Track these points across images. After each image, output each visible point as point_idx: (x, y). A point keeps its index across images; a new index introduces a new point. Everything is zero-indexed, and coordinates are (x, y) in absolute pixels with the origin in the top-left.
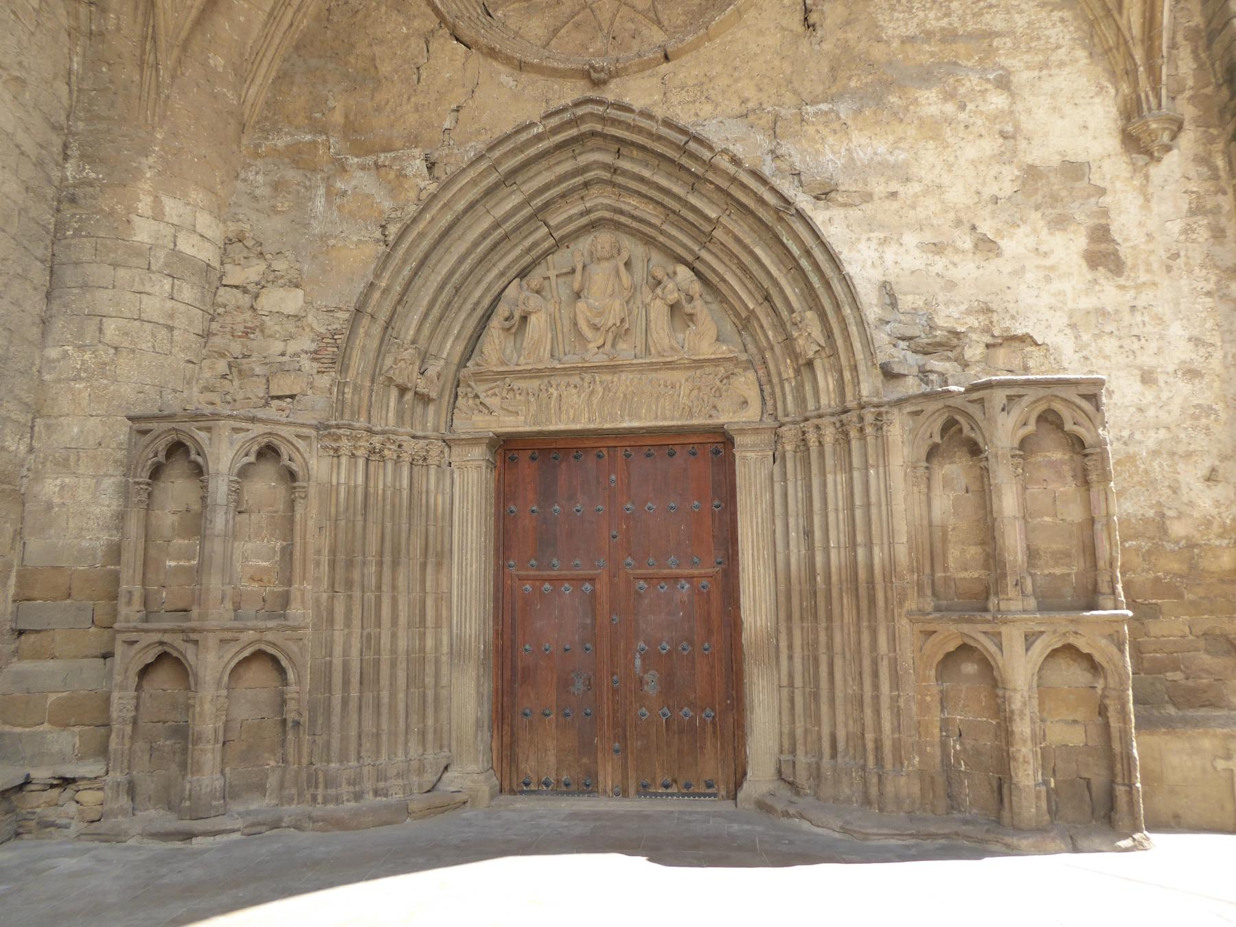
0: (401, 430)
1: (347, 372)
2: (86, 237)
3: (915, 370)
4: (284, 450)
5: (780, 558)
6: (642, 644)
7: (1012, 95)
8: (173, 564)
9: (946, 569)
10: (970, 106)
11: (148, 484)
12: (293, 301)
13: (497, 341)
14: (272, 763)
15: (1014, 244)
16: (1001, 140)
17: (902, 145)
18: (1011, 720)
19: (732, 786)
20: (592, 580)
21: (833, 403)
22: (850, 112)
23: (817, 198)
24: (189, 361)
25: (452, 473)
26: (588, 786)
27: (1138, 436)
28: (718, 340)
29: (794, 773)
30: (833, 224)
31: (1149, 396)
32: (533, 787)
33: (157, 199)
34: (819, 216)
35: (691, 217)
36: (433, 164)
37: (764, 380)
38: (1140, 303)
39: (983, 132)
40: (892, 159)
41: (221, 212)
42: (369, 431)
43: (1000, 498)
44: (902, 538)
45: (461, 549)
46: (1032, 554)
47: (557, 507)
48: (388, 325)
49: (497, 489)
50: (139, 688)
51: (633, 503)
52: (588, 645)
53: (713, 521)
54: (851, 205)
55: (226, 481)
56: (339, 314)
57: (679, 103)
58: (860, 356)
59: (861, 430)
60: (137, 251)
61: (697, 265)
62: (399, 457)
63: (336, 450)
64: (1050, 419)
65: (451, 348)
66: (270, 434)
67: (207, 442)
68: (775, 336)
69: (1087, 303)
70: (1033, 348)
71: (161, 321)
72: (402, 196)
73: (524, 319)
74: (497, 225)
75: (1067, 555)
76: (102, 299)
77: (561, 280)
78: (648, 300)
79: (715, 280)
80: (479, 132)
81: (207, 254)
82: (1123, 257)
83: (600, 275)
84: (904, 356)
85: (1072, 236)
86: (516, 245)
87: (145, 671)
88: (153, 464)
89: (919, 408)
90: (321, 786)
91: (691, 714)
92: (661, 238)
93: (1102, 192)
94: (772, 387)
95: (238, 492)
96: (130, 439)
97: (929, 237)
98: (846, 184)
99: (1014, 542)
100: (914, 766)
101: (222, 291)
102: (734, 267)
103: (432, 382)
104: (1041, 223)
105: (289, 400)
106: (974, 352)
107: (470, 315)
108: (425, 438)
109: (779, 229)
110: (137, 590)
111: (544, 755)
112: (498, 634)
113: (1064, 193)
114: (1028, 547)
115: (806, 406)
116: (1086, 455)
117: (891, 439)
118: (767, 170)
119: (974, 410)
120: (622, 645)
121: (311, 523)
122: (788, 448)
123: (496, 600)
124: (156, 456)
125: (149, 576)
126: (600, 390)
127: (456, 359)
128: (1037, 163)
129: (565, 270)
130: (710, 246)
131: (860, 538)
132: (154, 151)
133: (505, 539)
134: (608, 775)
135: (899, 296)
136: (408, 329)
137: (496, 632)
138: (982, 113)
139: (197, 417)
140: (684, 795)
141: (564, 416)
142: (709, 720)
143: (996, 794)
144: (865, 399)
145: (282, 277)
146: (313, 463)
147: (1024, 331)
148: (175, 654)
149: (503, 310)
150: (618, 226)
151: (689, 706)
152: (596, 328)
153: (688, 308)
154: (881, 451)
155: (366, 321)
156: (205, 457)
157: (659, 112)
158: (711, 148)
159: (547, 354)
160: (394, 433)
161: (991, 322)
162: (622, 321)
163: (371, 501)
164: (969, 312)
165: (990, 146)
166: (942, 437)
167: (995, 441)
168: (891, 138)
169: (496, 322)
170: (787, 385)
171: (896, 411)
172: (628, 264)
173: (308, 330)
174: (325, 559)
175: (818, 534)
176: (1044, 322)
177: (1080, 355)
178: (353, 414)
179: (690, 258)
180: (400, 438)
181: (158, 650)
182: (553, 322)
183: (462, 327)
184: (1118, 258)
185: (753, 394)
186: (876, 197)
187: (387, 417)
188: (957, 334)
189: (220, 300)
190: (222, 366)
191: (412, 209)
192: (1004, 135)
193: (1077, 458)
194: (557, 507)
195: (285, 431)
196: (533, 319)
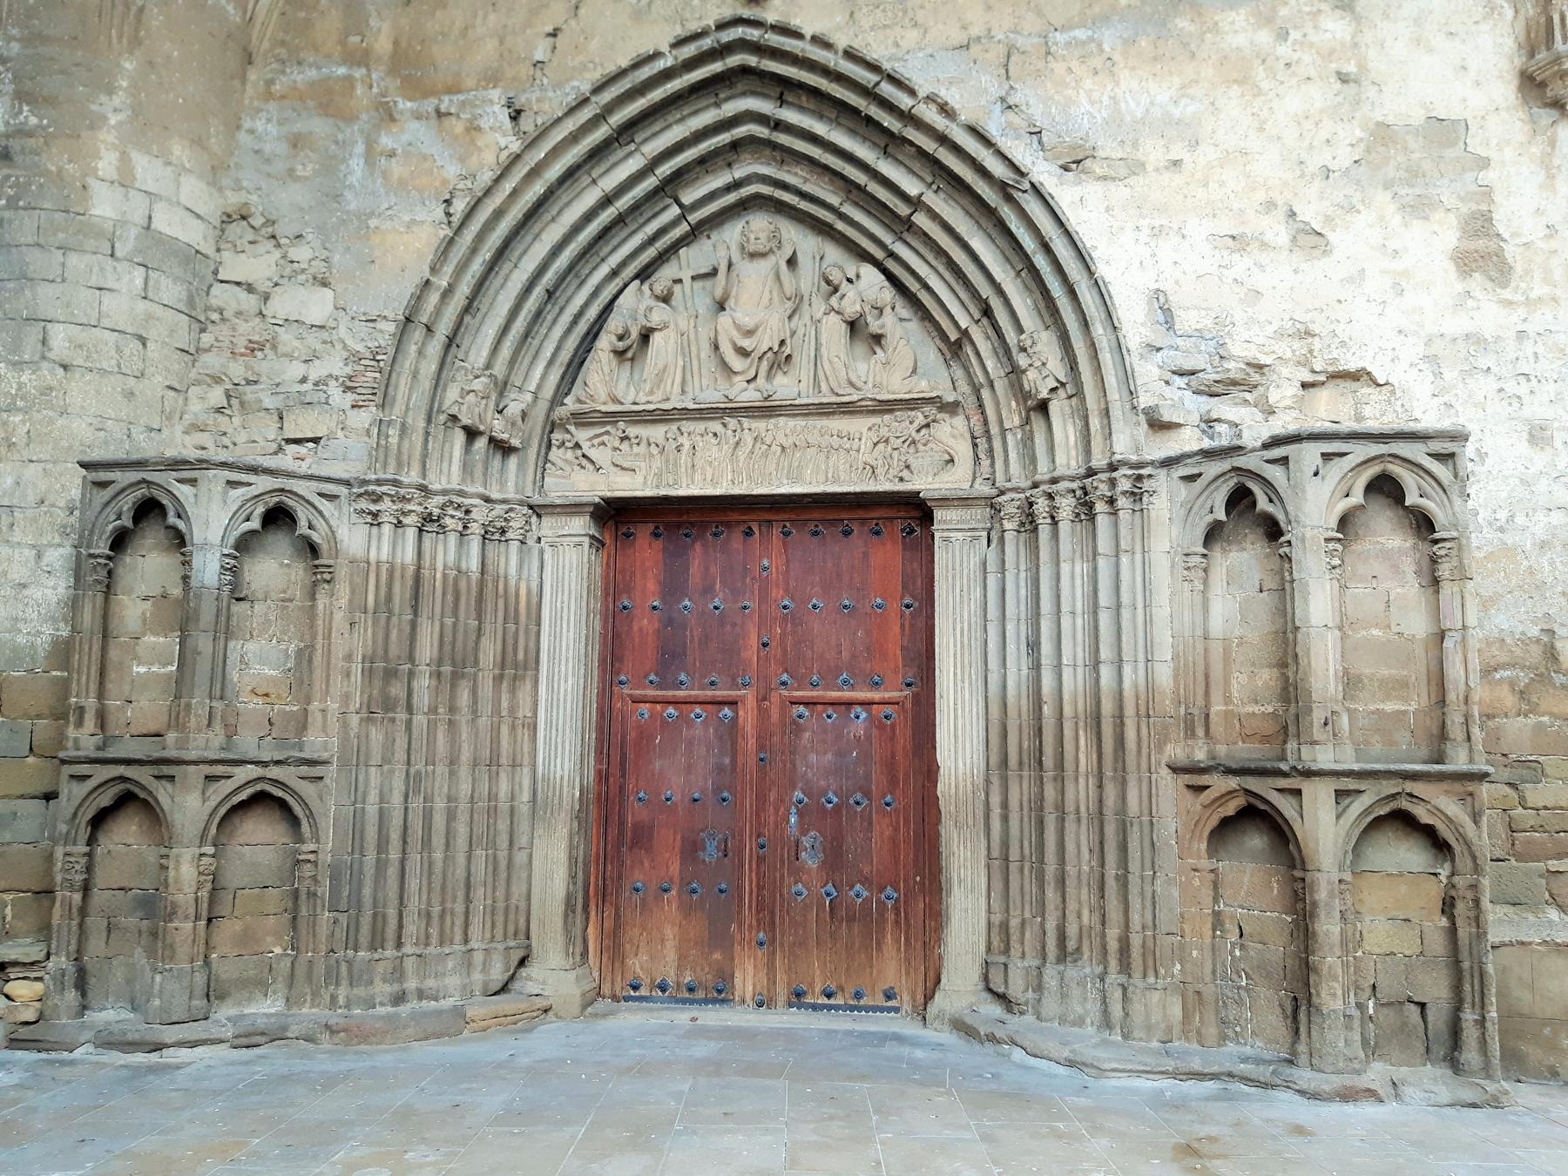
0: (470, 489)
1: (392, 405)
2: (25, 209)
3: (1195, 419)
4: (302, 515)
5: (994, 679)
6: (798, 794)
7: (1358, 19)
8: (142, 670)
9: (1228, 700)
10: (1294, 35)
11: (109, 558)
12: (318, 304)
13: (607, 370)
14: (278, 950)
15: (1354, 239)
16: (1338, 85)
17: (1191, 91)
18: (1313, 915)
19: (920, 999)
20: (733, 703)
21: (1073, 463)
22: (1119, 42)
23: (1066, 168)
24: (170, 388)
25: (542, 552)
26: (720, 992)
27: (1520, 520)
28: (914, 371)
29: (1006, 981)
30: (1083, 205)
31: (1540, 459)
32: (643, 992)
33: (124, 158)
34: (1065, 193)
35: (882, 194)
36: (519, 112)
37: (978, 431)
38: (1531, 328)
39: (1313, 73)
40: (1176, 112)
41: (215, 173)
42: (423, 488)
43: (1306, 601)
44: (1164, 653)
45: (552, 658)
46: (1351, 683)
47: (687, 603)
48: (451, 341)
49: (605, 578)
50: (91, 841)
51: (793, 599)
52: (725, 794)
53: (902, 626)
54: (1113, 179)
55: (218, 555)
56: (382, 325)
57: (872, 28)
58: (1114, 394)
59: (1111, 501)
60: (91, 230)
61: (891, 265)
62: (465, 527)
63: (375, 515)
64: (1385, 488)
65: (540, 376)
66: (282, 490)
67: (192, 500)
68: (995, 368)
69: (1457, 325)
70: (1370, 390)
71: (129, 330)
72: (474, 158)
73: (645, 337)
74: (607, 201)
75: (1403, 684)
76: (46, 298)
77: (699, 285)
78: (819, 315)
79: (913, 286)
80: (584, 68)
81: (194, 234)
82: (1510, 260)
83: (754, 281)
84: (1181, 399)
85: (1436, 228)
86: (634, 232)
87: (100, 820)
88: (115, 529)
89: (1195, 471)
90: (344, 983)
91: (866, 894)
92: (840, 226)
93: (1484, 163)
94: (989, 439)
95: (233, 570)
96: (83, 495)
97: (1226, 226)
98: (1108, 147)
99: (1324, 664)
100: (1173, 976)
101: (217, 289)
102: (941, 269)
103: (513, 424)
104: (1392, 208)
105: (311, 445)
106: (1283, 392)
107: (569, 331)
108: (504, 501)
109: (1006, 212)
110: (91, 703)
111: (661, 949)
112: (602, 777)
113: (1427, 165)
114: (1346, 672)
115: (1035, 468)
116: (1436, 542)
117: (1153, 514)
118: (993, 130)
119: (1275, 474)
120: (772, 796)
121: (339, 616)
122: (1007, 525)
123: (600, 729)
124: (119, 518)
125: (109, 686)
126: (750, 442)
127: (548, 392)
128: (1390, 120)
129: (703, 271)
130: (906, 236)
131: (1105, 653)
132: (120, 87)
133: (613, 650)
134: (747, 979)
135: (1176, 312)
136: (479, 351)
137: (599, 773)
138: (1312, 45)
139: (176, 464)
140: (852, 1008)
141: (698, 477)
142: (890, 904)
143: (1289, 1021)
144: (1117, 457)
145: (303, 271)
146: (343, 533)
147: (1359, 365)
148: (142, 795)
149: (614, 323)
150: (781, 208)
151: (863, 884)
152: (743, 353)
153: (874, 326)
154: (1139, 530)
155: (418, 334)
156: (188, 521)
157: (842, 42)
158: (912, 92)
159: (677, 388)
160: (461, 493)
161: (1311, 351)
162: (782, 343)
163: (426, 589)
164: (1280, 335)
165: (1320, 95)
166: (1228, 513)
167: (1302, 518)
168: (1177, 81)
169: (605, 342)
170: (1009, 437)
171: (1163, 472)
172: (792, 262)
173: (339, 346)
174: (357, 669)
175: (1046, 648)
176: (1390, 353)
177: (1441, 400)
178: (399, 465)
179: (879, 254)
180: (467, 501)
181: (119, 788)
182: (685, 350)
183: (558, 349)
184: (1503, 261)
185: (963, 450)
186: (1150, 168)
187: (448, 472)
188: (1260, 367)
189: (214, 302)
190: (216, 396)
191: (486, 177)
192: (1344, 79)
193: (1424, 547)
194: (687, 603)
195: (300, 487)
196: (656, 339)
